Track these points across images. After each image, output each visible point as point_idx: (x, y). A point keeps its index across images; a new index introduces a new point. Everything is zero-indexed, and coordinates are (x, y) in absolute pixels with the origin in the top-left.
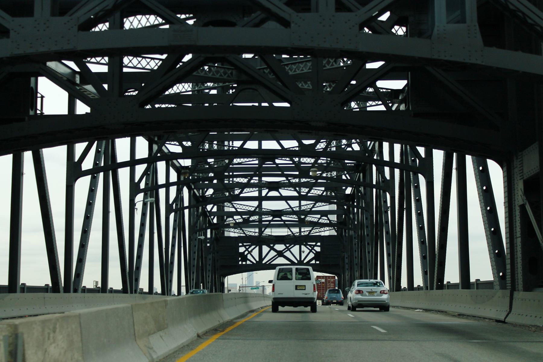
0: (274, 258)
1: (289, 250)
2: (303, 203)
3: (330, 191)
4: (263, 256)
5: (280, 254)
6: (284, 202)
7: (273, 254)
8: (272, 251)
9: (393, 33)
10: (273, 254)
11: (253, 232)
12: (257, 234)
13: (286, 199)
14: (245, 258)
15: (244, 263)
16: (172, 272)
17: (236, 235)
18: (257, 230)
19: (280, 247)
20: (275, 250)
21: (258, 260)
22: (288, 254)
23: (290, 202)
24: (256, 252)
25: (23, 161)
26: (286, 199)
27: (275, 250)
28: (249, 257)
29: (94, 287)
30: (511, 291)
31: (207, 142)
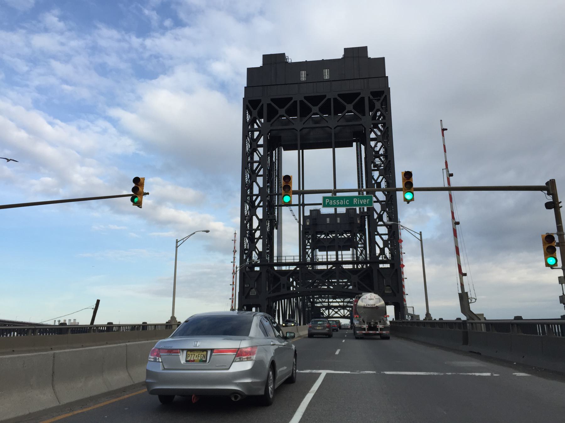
0: (334, 314)
1: (339, 311)
2: (344, 303)
3: (332, 239)
4: (330, 314)
5: (336, 312)
6: (338, 303)
7: (334, 312)
8: (333, 311)
9: (333, 214)
10: (334, 312)
11: (326, 304)
12: (327, 305)
13: (338, 302)
14: (323, 314)
15: (323, 316)
16: (295, 316)
17: (320, 305)
18: (327, 304)
19: (336, 310)
20: (334, 311)
21: (328, 315)
22: (339, 312)
23: (339, 303)
24: (327, 312)
25: (231, 339)
26: (338, 302)
27: (334, 311)
28: (324, 314)
29: (284, 256)
30: (285, 149)
31: (311, 266)
